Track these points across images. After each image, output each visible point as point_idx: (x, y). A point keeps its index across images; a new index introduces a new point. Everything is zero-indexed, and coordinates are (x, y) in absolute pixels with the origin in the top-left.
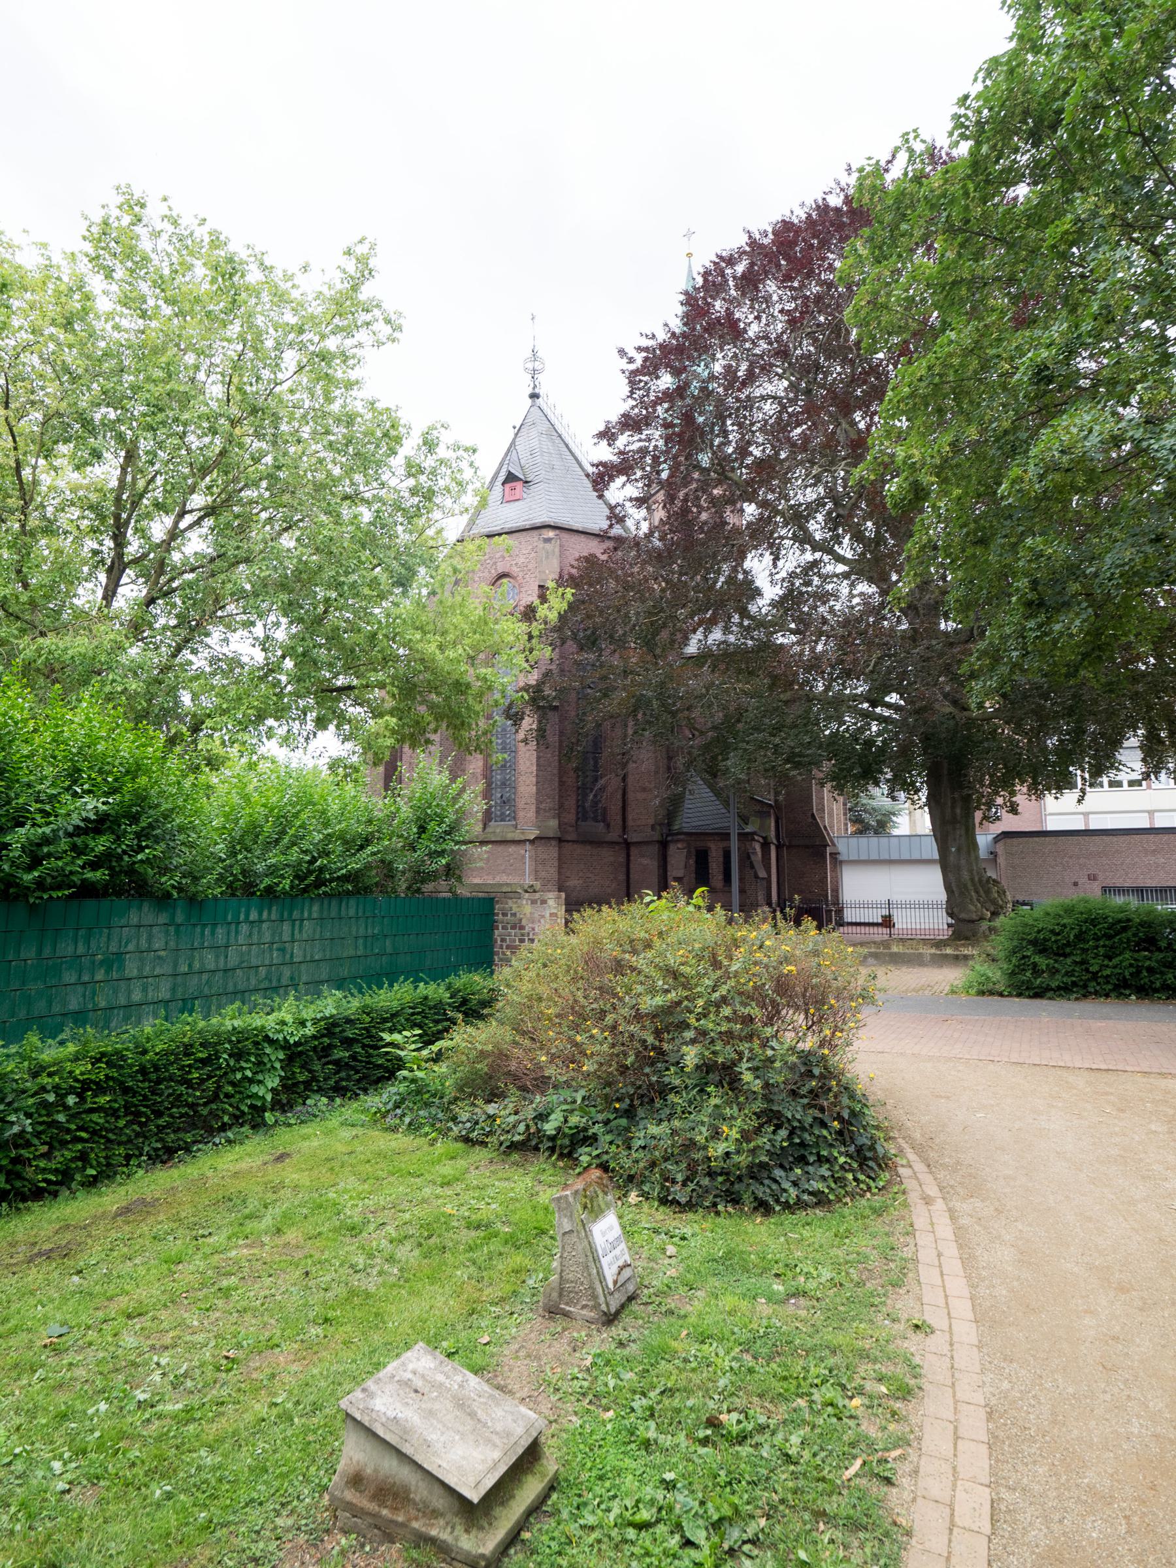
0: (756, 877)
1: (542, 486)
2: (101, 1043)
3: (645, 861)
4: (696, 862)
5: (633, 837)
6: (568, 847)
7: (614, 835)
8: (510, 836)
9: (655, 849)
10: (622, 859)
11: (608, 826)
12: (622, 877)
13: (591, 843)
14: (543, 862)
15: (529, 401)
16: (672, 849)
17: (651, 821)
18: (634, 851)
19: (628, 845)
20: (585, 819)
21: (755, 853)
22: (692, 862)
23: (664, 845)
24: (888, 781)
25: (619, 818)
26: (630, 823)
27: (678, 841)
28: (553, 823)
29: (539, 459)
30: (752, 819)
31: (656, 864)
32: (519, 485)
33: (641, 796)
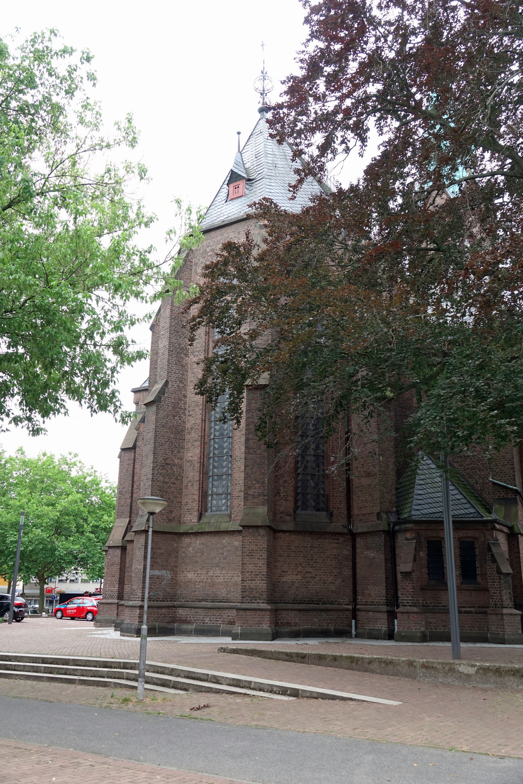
0: (499, 572)
1: (265, 181)
2: (478, 558)
3: (372, 554)
4: (428, 555)
5: (359, 527)
6: (284, 539)
7: (338, 525)
8: (224, 526)
9: (380, 540)
10: (347, 552)
11: (331, 515)
12: (348, 572)
13: (312, 533)
14: (251, 554)
15: (259, 116)
16: (401, 539)
17: (377, 509)
18: (360, 542)
19: (353, 536)
20: (305, 507)
21: (497, 545)
22: (423, 554)
23: (391, 535)
24: (19, 302)
25: (343, 506)
26: (355, 511)
27: (406, 530)
28: (263, 510)
29: (263, 160)
30: (496, 506)
31: (383, 557)
32: (242, 184)
33: (365, 481)
